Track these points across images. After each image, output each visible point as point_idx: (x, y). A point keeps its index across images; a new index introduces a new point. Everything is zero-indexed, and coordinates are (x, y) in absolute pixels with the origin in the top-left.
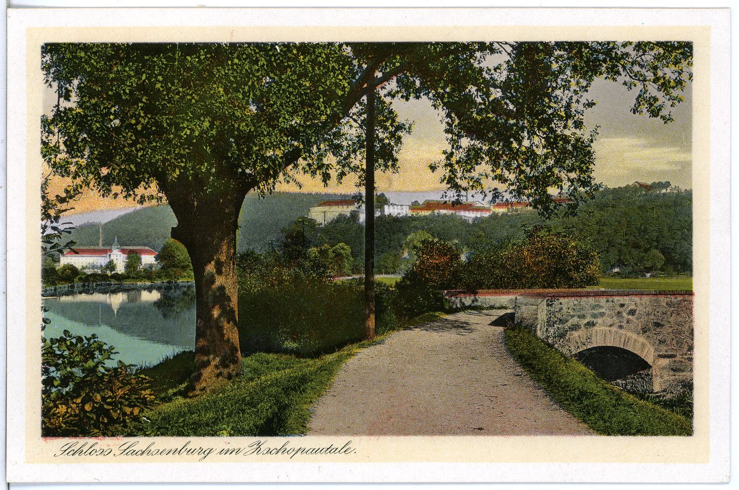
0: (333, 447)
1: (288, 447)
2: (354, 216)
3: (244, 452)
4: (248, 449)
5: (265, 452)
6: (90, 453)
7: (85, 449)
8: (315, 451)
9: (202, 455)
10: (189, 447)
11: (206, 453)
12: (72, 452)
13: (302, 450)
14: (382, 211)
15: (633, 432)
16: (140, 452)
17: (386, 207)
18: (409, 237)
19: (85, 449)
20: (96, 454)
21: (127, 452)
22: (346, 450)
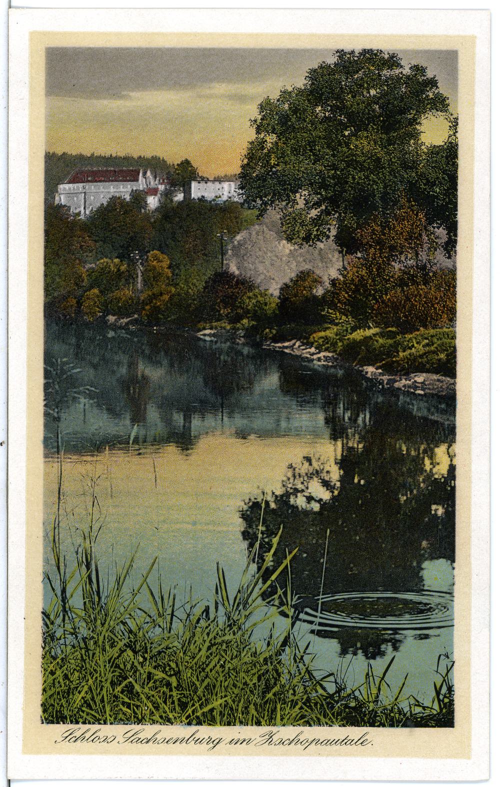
0: (348, 738)
1: (302, 738)
2: (138, 198)
3: (254, 742)
4: (259, 739)
5: (277, 743)
6: (93, 740)
7: (87, 735)
8: (329, 742)
9: (211, 745)
10: (197, 736)
11: (215, 743)
12: (74, 739)
13: (317, 742)
14: (187, 191)
15: (376, 724)
16: (145, 740)
17: (194, 185)
18: (238, 237)
19: (87, 735)
20: (99, 741)
21: (134, 740)
22: (362, 742)
